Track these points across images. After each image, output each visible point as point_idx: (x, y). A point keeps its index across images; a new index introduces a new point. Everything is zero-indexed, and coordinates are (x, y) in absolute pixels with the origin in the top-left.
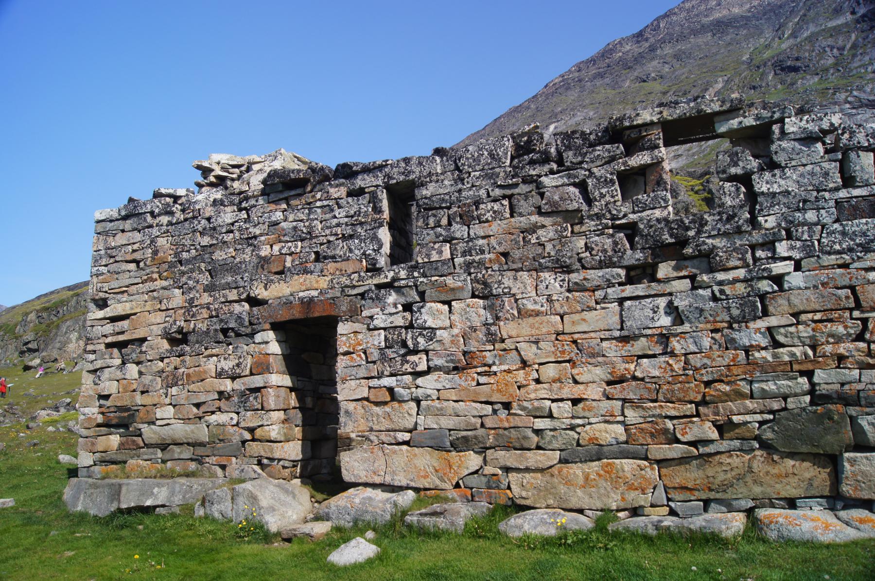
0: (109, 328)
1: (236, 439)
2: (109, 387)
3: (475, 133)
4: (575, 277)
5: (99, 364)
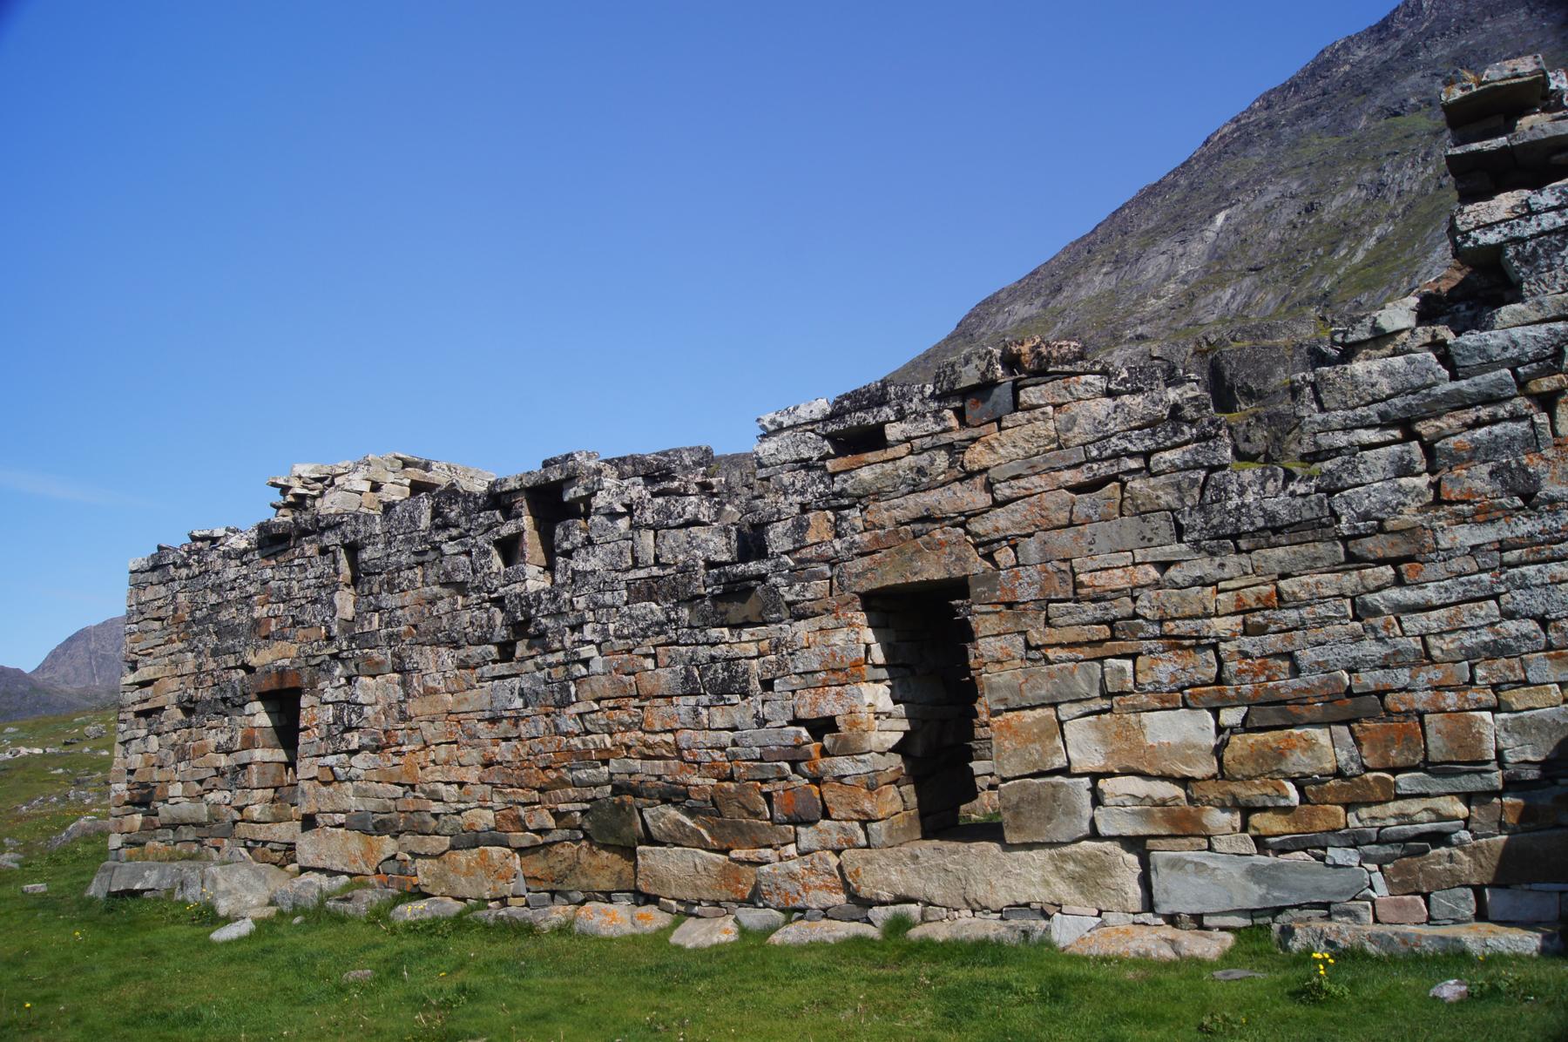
0: (137, 695)
1: (228, 820)
2: (136, 761)
3: (1077, 241)
4: (461, 653)
5: (128, 735)
